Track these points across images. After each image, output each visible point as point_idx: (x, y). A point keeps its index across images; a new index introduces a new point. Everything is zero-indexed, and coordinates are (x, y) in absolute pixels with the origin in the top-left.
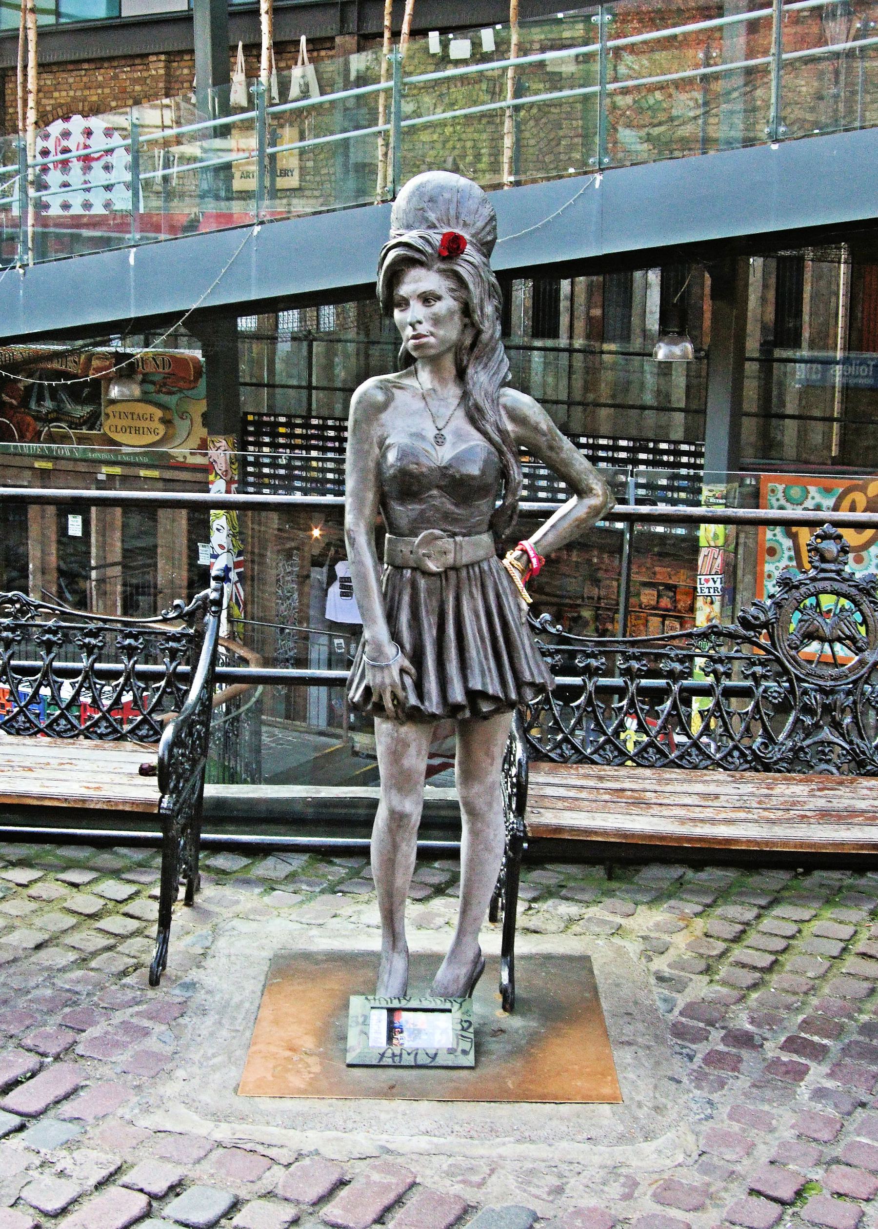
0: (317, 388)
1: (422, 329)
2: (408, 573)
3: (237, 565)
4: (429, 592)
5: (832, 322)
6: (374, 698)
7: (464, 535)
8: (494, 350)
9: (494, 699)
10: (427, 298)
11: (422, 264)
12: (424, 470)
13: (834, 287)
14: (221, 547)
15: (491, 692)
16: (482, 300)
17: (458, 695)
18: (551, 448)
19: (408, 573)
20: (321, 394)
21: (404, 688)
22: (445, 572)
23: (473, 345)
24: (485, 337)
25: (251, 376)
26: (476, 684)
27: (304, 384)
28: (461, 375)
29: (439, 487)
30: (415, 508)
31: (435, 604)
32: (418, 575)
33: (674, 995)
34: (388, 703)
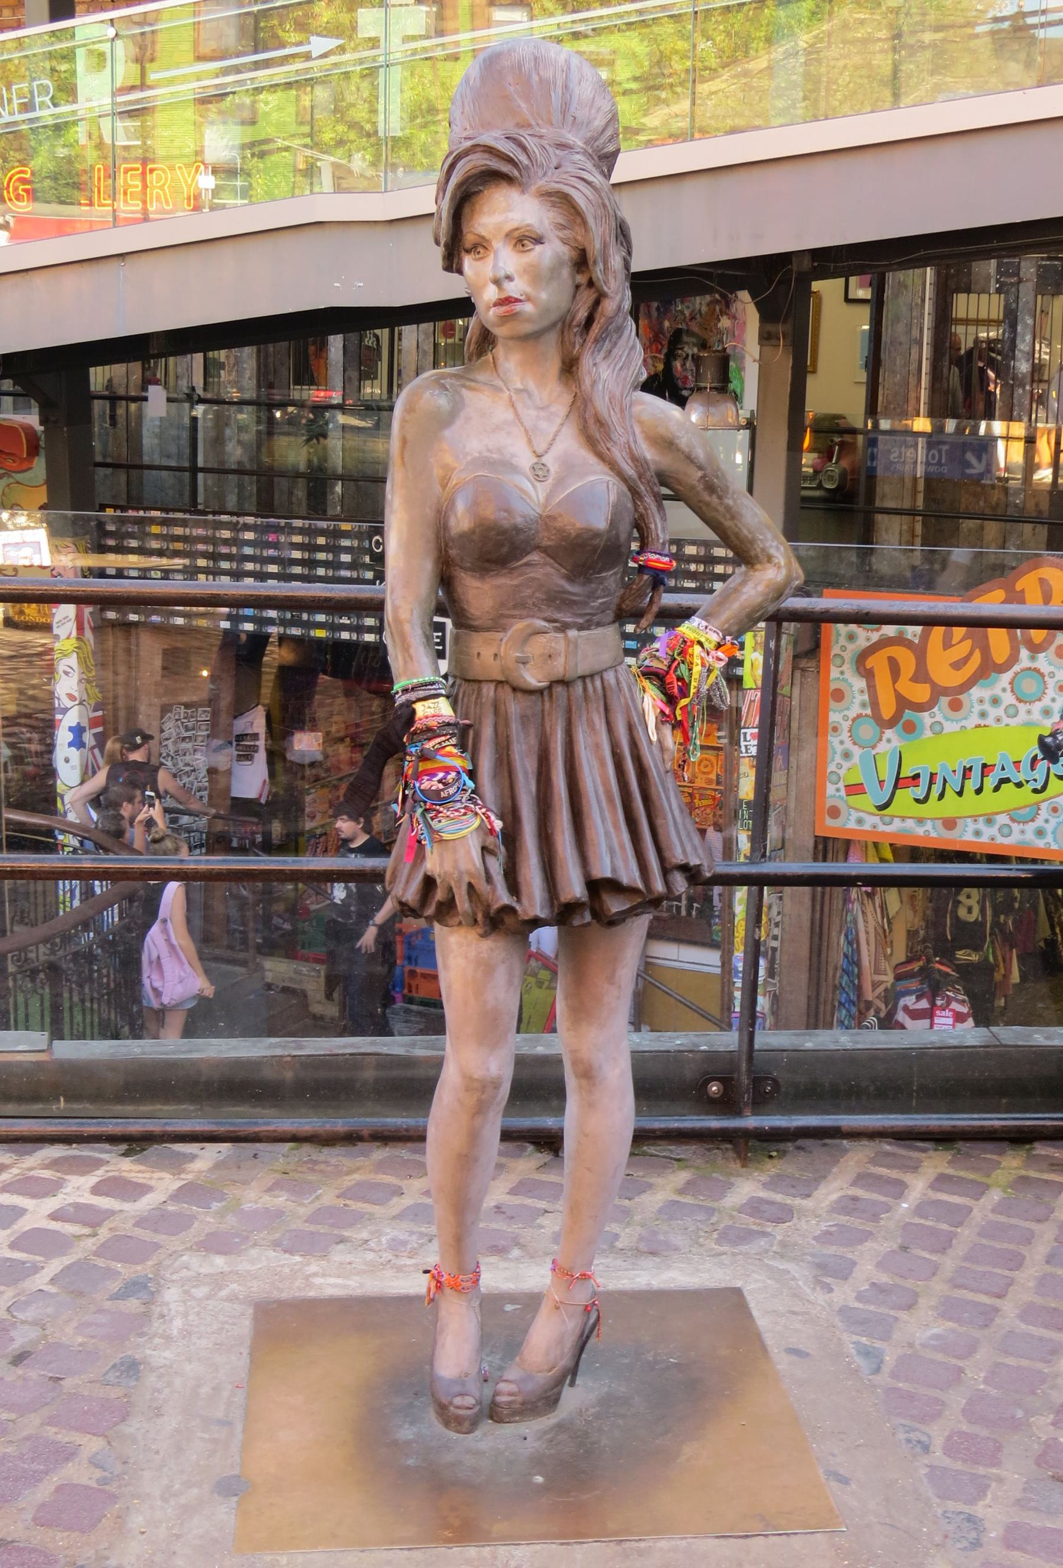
0: (202, 470)
1: (513, 289)
2: (489, 691)
3: (94, 723)
4: (524, 719)
5: (913, 381)
6: (440, 895)
7: (581, 628)
8: (620, 330)
9: (632, 891)
10: (524, 239)
11: (509, 179)
12: (519, 520)
13: (915, 333)
14: (71, 697)
15: (625, 881)
16: (605, 246)
17: (574, 888)
18: (711, 488)
19: (489, 691)
20: (211, 479)
21: (489, 879)
22: (550, 687)
23: (590, 321)
24: (609, 306)
25: (104, 456)
26: (603, 869)
27: (187, 464)
28: (569, 367)
29: (545, 550)
30: (504, 582)
31: (533, 741)
32: (506, 693)
33: (878, 1344)
34: (463, 903)
